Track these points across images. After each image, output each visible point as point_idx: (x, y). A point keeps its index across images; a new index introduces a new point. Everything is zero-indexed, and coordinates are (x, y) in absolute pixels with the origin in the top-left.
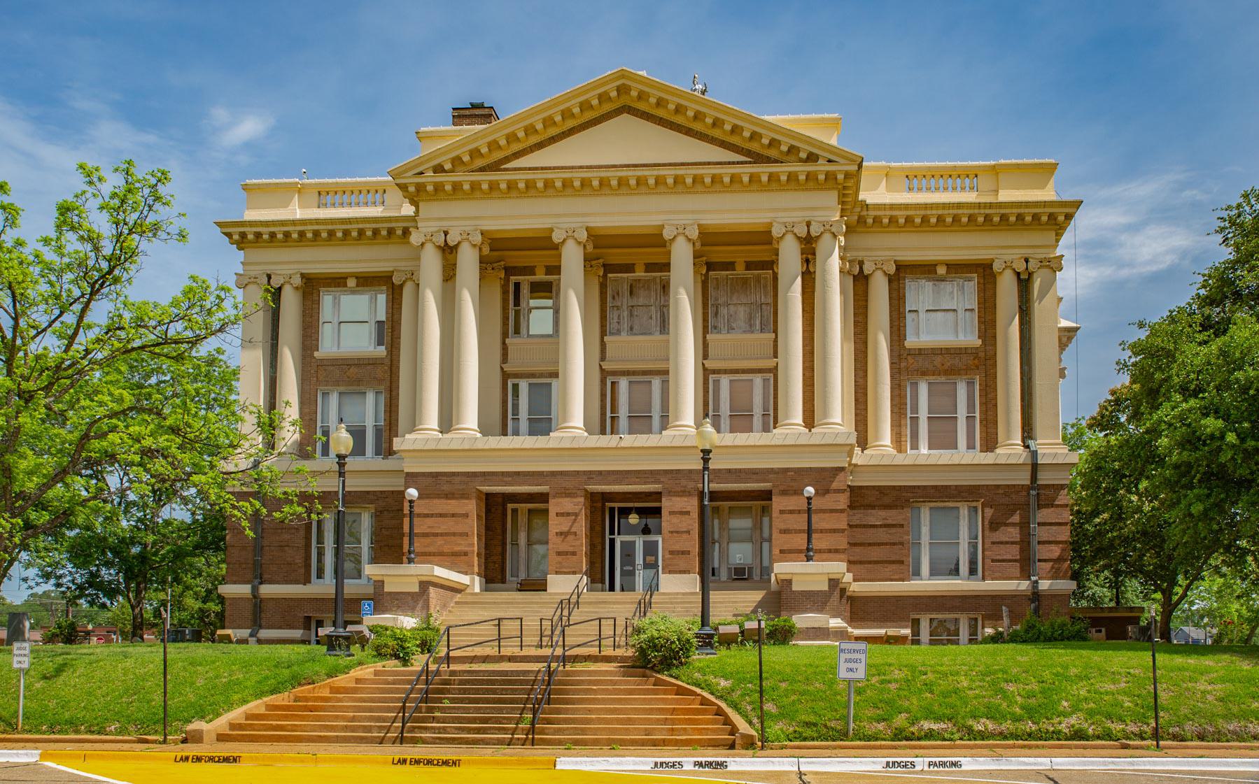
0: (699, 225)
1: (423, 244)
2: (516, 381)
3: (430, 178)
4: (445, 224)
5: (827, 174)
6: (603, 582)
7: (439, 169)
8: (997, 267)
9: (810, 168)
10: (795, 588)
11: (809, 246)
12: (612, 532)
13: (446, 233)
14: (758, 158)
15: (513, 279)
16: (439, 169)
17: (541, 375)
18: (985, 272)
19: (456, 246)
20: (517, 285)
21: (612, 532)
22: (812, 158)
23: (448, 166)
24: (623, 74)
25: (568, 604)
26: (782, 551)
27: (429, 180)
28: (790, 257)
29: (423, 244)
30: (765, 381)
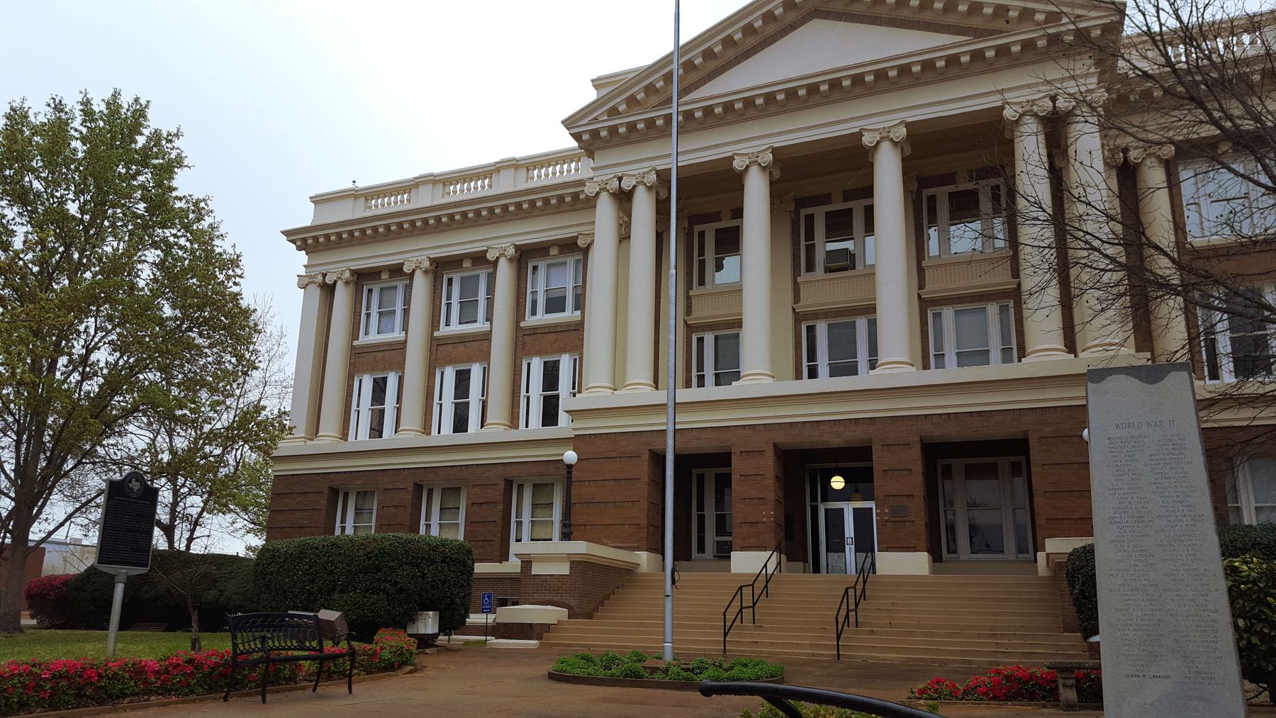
6: (805, 560)
11: (1056, 128)
12: (814, 499)
16: (613, 112)
21: (814, 499)
25: (763, 584)
29: (598, 194)
30: (1004, 309)
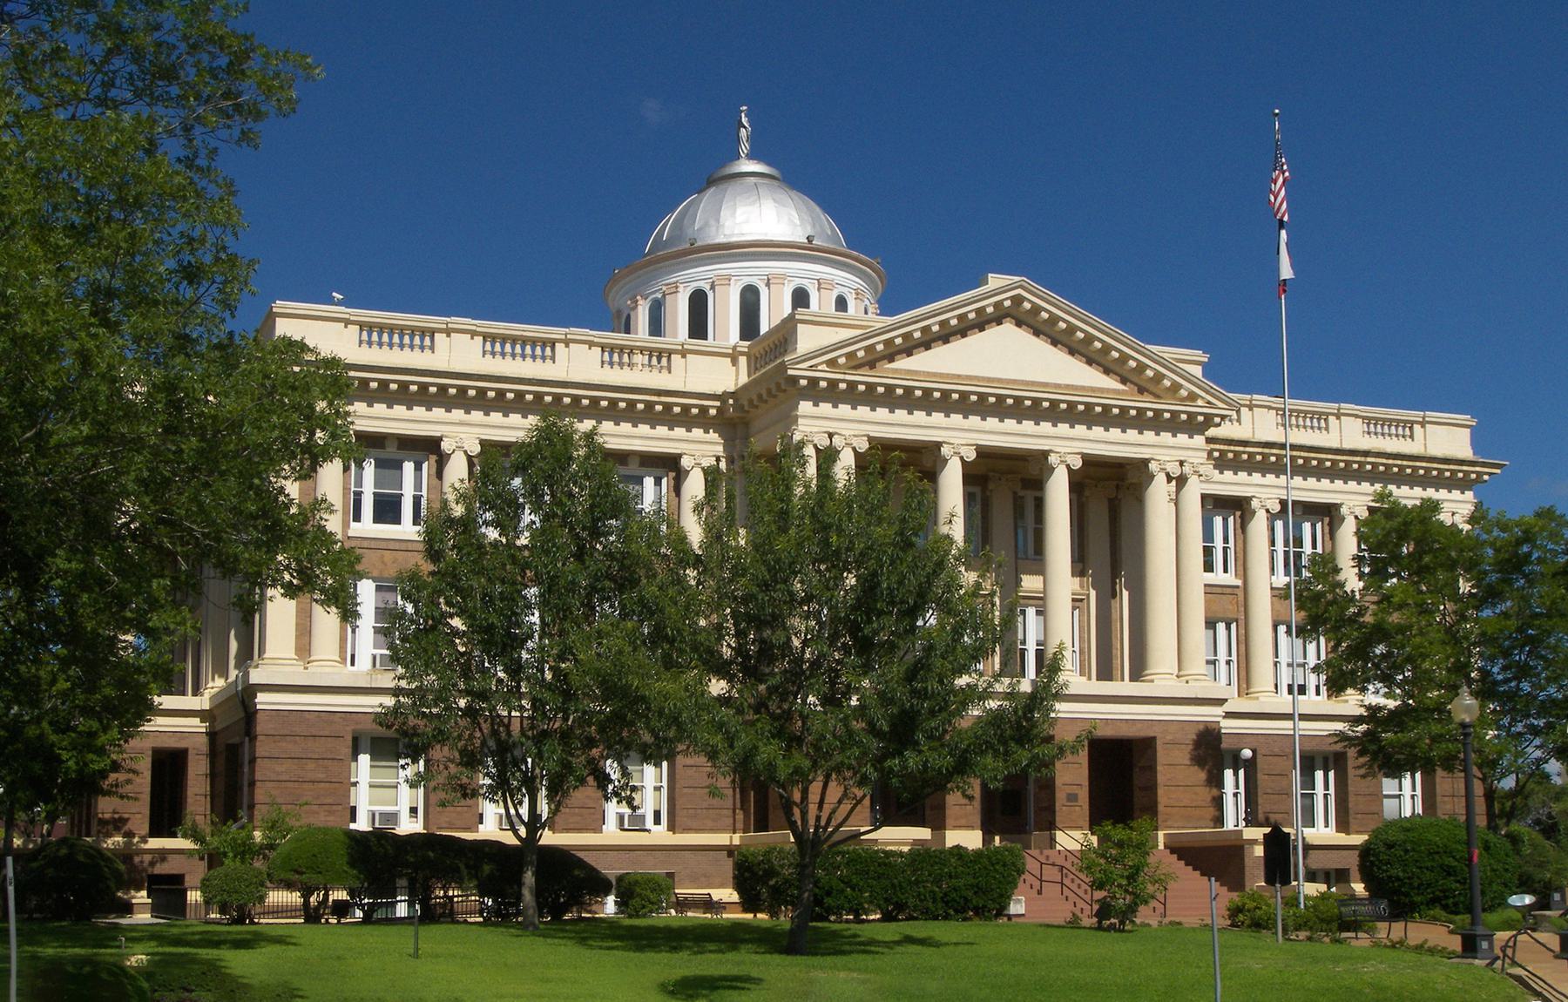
13: (831, 436)
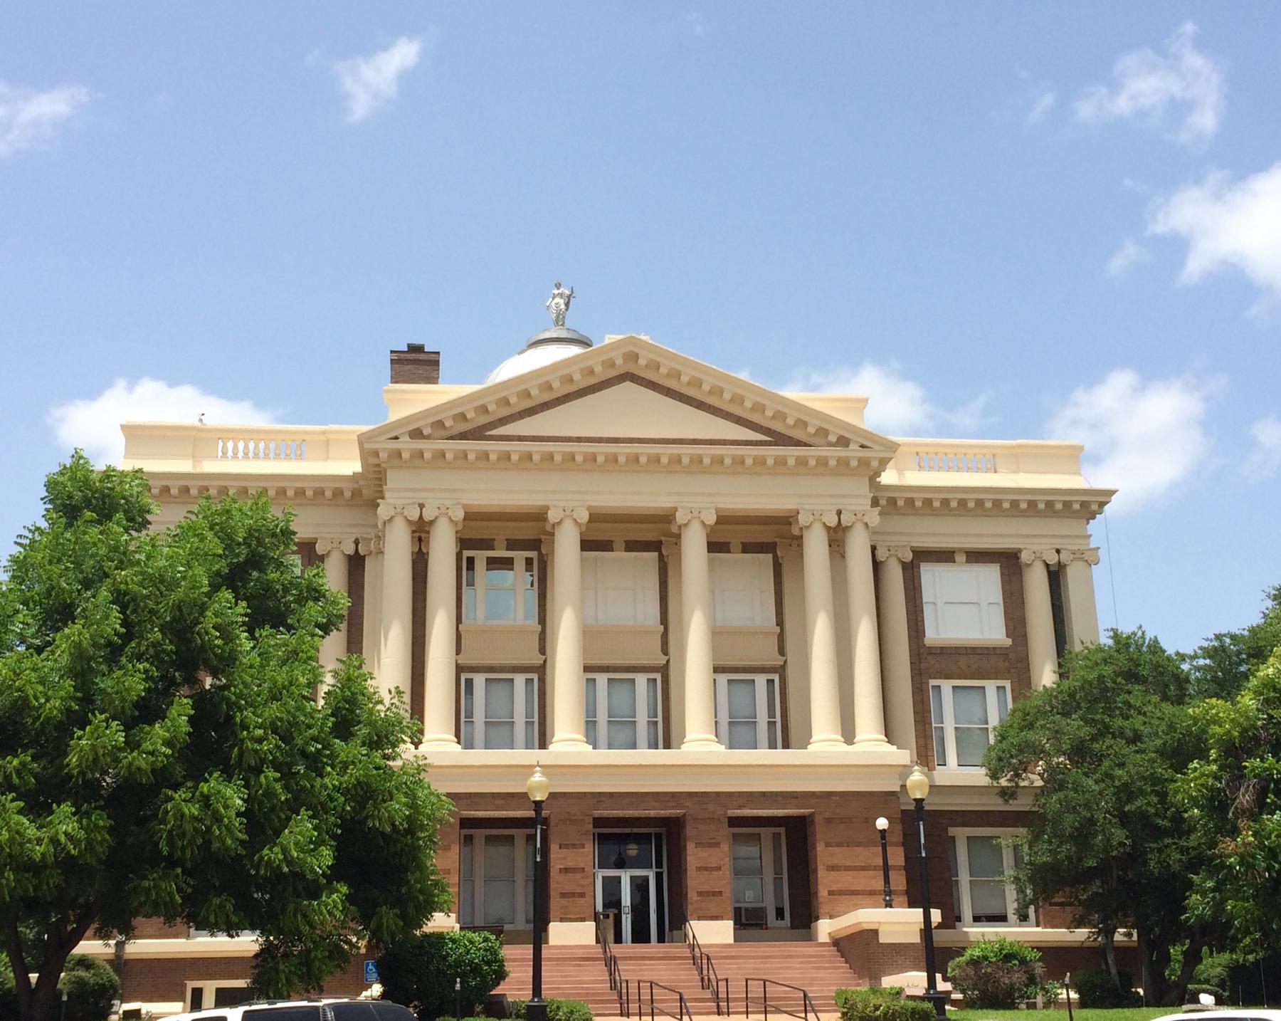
0: (717, 510)
1: (390, 520)
2: (469, 676)
3: (407, 445)
4: (420, 497)
5: (860, 460)
7: (417, 434)
8: (1025, 557)
9: (840, 452)
10: (883, 939)
11: (837, 538)
13: (421, 506)
14: (780, 439)
15: (467, 553)
16: (417, 434)
17: (502, 669)
18: (1010, 563)
19: (432, 523)
20: (471, 561)
22: (843, 442)
23: (426, 431)
24: (632, 341)
26: (831, 893)
27: (407, 446)
28: (816, 548)
29: (390, 520)
